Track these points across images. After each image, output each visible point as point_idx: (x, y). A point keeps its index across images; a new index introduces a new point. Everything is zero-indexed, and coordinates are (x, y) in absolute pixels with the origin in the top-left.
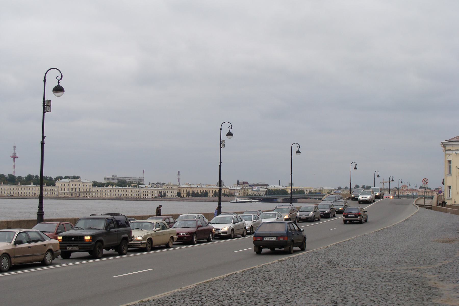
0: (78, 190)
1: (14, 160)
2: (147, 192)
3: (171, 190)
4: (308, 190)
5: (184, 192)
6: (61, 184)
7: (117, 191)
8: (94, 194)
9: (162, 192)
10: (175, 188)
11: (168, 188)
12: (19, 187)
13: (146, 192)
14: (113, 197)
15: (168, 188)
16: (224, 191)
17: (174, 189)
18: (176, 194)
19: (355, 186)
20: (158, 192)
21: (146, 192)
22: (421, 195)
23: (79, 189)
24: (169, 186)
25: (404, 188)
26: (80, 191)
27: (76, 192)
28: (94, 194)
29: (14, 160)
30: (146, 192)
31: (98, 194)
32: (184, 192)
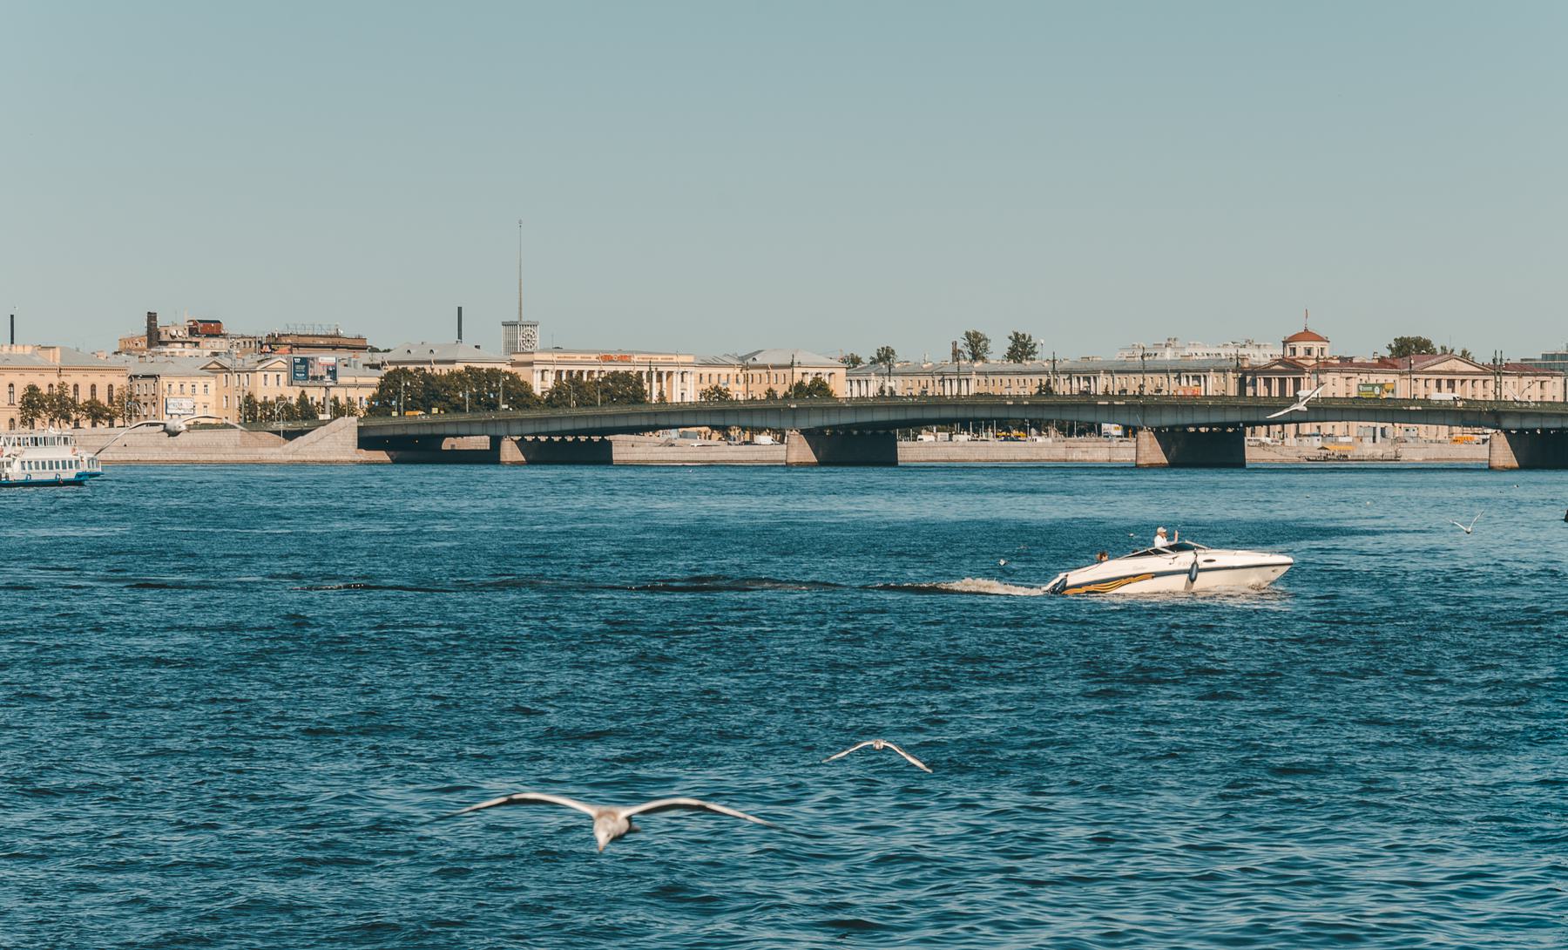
25: (1300, 353)
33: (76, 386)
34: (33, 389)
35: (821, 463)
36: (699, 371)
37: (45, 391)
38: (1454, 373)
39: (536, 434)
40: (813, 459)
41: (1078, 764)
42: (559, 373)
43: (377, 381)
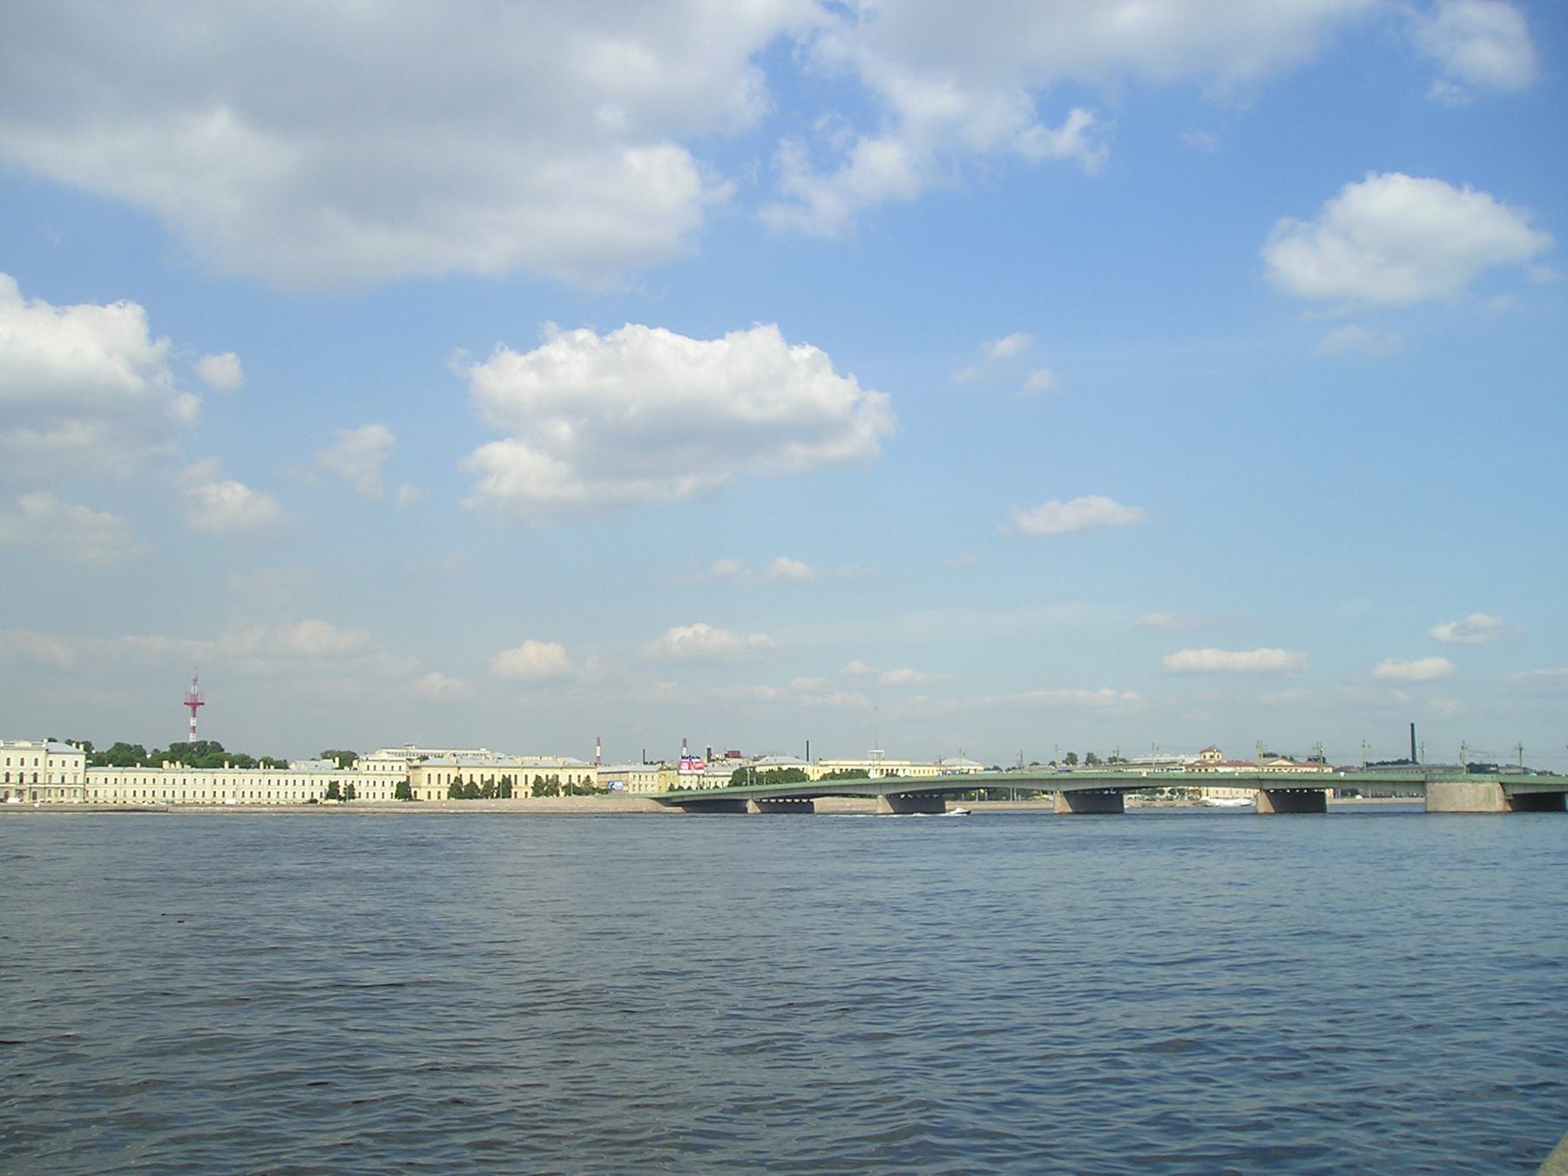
0: (28, 779)
1: (194, 710)
2: (291, 783)
3: (381, 775)
4: (882, 770)
5: (429, 782)
6: (64, 762)
7: (179, 781)
8: (91, 794)
9: (340, 784)
10: (396, 768)
11: (372, 768)
12: (270, 777)
13: (286, 784)
14: (125, 802)
15: (372, 768)
16: (570, 776)
17: (392, 773)
18: (394, 790)
19: (1065, 757)
20: (326, 784)
21: (289, 782)
22: (175, 764)
23: (35, 775)
24: (375, 763)
25: (1208, 757)
26: (39, 781)
27: (21, 787)
28: (91, 794)
29: (194, 710)
30: (286, 784)
31: (105, 791)
32: (429, 782)
33: (516, 776)
34: (538, 778)
35: (1514, 811)
36: (910, 768)
37: (544, 778)
38: (1281, 766)
39: (769, 798)
40: (1273, 811)
41: (1163, 886)
42: (887, 770)
43: (731, 774)
